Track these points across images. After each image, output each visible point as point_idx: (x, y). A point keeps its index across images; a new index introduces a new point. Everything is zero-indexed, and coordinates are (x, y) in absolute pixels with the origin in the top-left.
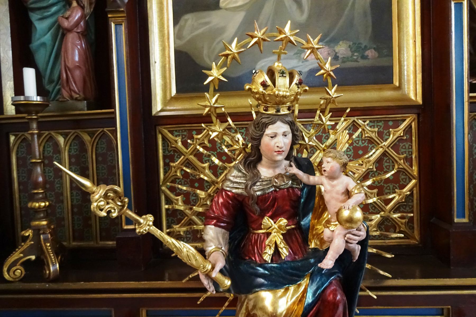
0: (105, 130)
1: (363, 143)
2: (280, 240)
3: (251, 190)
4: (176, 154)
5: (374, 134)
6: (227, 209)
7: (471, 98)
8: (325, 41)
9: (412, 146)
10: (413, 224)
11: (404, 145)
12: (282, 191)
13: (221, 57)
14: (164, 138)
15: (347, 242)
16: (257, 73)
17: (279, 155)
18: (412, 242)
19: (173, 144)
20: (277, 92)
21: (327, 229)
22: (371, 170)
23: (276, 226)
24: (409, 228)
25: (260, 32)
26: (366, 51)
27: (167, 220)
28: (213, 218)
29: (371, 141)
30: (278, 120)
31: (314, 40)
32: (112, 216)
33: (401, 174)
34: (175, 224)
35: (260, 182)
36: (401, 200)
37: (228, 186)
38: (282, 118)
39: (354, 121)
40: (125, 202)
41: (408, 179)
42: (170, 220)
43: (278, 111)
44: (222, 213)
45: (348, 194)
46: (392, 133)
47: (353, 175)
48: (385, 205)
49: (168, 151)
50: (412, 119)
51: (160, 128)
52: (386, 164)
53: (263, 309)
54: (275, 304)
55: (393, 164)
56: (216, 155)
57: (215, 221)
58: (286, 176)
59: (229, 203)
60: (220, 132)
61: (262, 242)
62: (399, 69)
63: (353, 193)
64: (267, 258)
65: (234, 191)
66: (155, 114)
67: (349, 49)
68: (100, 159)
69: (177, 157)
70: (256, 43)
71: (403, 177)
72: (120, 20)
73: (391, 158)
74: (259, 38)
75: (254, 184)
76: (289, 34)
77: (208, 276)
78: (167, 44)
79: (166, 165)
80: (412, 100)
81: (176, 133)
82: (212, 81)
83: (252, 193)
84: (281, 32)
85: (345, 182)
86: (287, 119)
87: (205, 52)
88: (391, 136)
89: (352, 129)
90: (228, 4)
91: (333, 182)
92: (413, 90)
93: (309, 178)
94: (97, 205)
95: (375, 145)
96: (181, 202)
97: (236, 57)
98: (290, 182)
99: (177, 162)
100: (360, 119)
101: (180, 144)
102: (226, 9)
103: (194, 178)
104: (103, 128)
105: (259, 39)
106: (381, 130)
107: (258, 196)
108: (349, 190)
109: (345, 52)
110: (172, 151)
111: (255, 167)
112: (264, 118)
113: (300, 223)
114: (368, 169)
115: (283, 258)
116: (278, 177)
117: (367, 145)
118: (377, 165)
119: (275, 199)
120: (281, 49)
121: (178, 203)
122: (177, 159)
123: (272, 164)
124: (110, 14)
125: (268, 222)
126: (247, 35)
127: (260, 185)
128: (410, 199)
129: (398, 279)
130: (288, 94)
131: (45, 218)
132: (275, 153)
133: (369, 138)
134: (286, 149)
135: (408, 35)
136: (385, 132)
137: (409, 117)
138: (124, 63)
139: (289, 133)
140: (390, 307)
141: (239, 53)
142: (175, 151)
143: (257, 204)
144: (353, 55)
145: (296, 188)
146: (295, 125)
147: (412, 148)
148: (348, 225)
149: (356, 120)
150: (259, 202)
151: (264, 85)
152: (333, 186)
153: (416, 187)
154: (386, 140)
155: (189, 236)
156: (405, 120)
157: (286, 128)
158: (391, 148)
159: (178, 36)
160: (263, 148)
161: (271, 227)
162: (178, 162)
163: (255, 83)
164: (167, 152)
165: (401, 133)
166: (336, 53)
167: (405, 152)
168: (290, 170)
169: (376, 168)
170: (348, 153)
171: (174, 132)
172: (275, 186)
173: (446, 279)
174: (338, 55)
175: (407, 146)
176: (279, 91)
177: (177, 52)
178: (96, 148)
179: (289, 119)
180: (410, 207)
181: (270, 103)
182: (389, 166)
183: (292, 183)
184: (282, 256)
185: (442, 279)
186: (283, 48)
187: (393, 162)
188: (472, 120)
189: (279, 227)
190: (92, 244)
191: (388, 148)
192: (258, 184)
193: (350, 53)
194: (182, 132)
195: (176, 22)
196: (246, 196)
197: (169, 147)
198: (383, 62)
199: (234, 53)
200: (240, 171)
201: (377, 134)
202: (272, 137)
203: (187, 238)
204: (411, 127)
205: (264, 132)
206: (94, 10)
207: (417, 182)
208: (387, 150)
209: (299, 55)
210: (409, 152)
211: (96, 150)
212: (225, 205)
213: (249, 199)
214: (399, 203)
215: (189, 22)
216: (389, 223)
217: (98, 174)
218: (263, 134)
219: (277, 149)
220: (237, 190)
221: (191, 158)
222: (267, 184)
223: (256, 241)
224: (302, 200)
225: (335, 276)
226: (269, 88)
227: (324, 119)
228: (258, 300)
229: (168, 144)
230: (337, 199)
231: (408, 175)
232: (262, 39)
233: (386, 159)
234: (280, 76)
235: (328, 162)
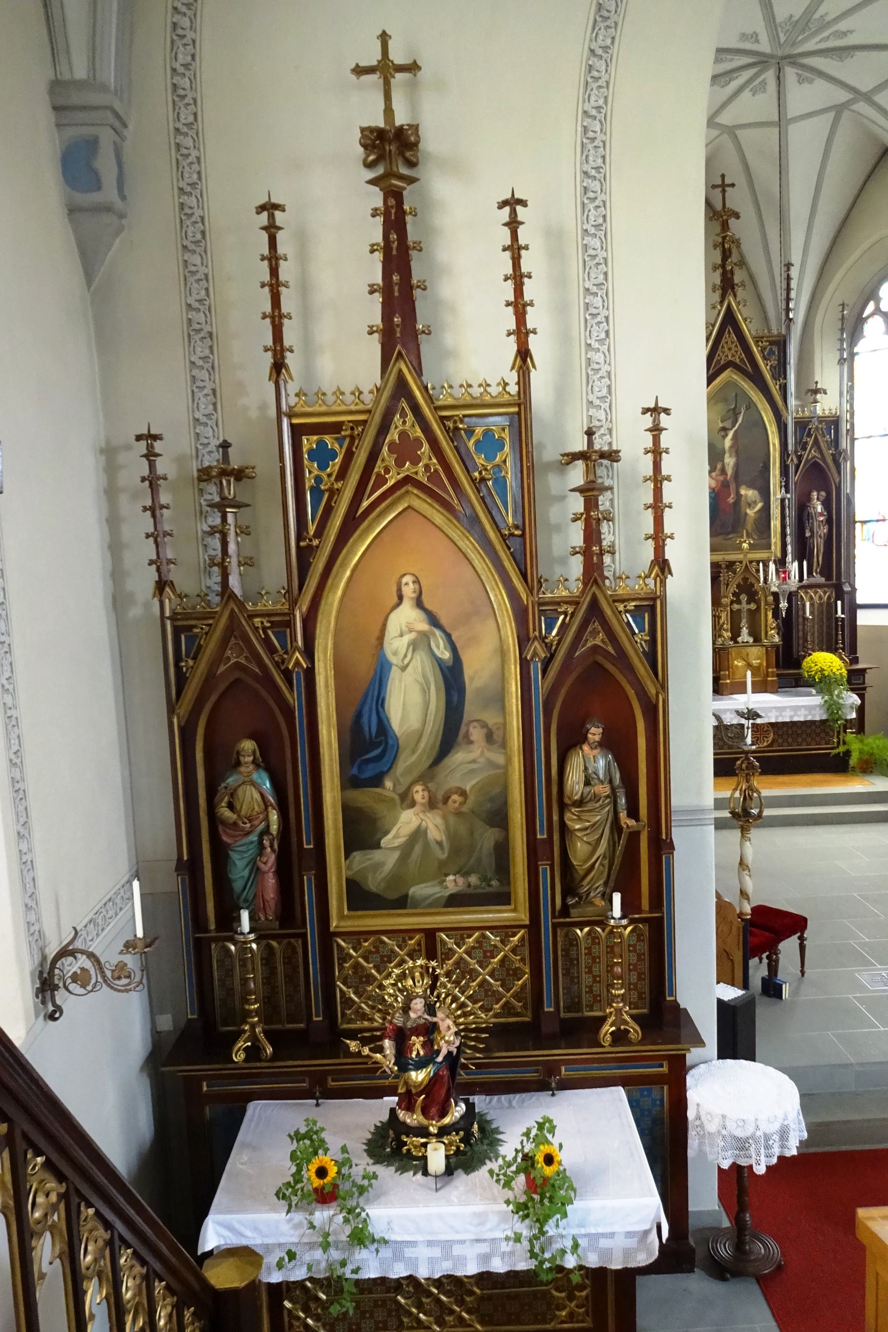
18: (527, 1019)
37: (395, 1021)
53: (412, 1079)
64: (414, 1056)
79: (340, 965)
87: (370, 878)
131: (256, 1016)
159: (349, 868)
177: (347, 879)
190: (279, 1027)
193: (479, 883)
195: (346, 859)
198: (504, 889)
212: (393, 1029)
228: (409, 1077)
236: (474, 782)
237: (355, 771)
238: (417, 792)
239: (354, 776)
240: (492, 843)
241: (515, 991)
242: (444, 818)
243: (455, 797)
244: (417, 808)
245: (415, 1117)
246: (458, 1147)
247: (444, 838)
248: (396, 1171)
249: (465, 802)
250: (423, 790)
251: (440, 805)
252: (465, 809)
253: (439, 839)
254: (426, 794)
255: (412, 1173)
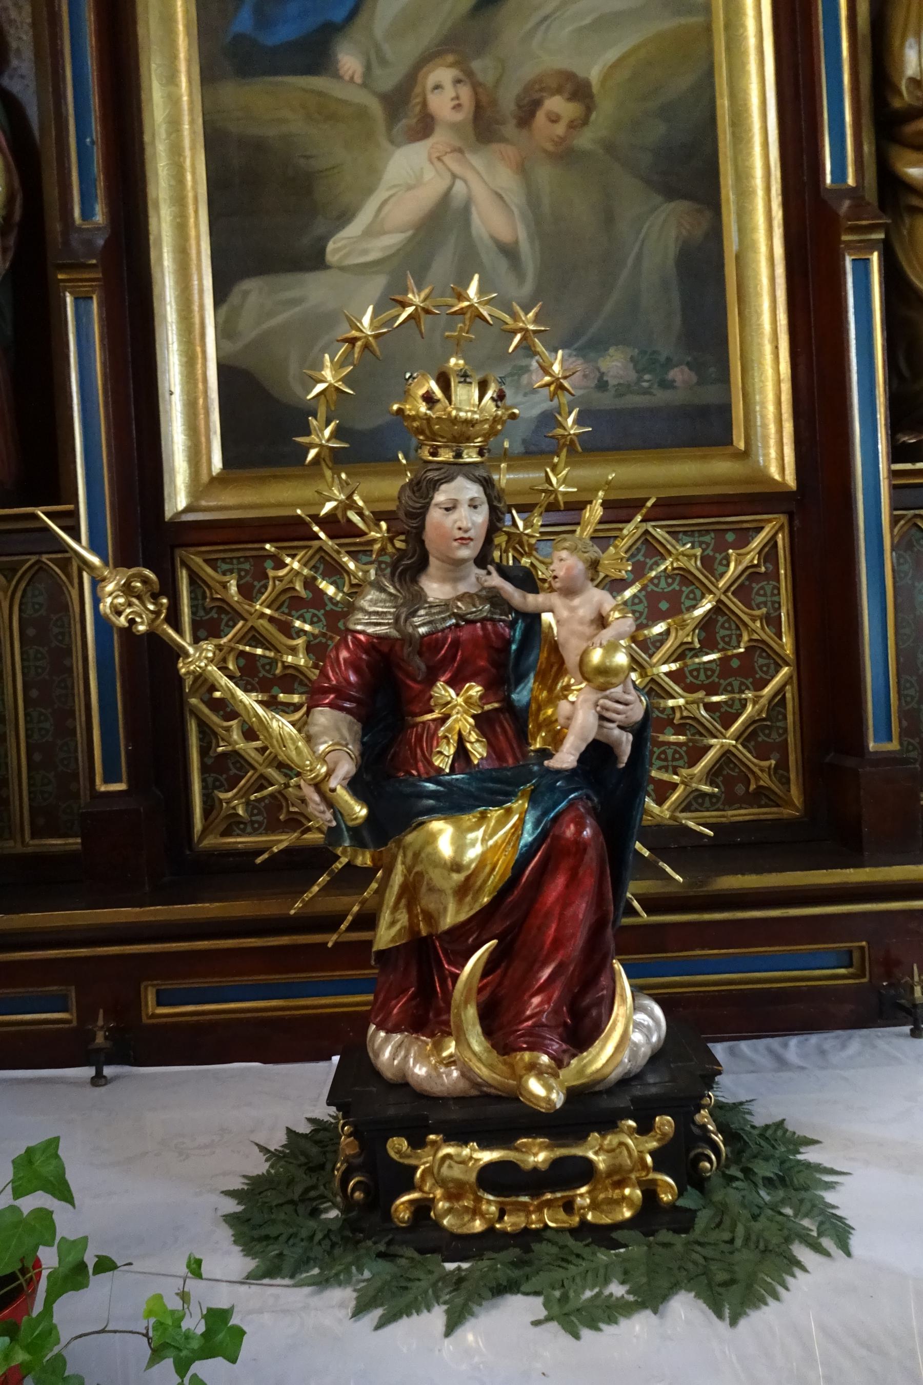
0: (44, 558)
1: (669, 585)
2: (468, 727)
3: (408, 624)
4: (223, 616)
5: (693, 562)
6: (357, 671)
7: (894, 474)
8: (576, 346)
9: (779, 589)
10: (788, 770)
11: (762, 588)
12: (470, 627)
13: (341, 344)
14: (195, 580)
15: (602, 718)
16: (414, 378)
17: (463, 547)
18: (787, 812)
19: (217, 593)
20: (454, 413)
21: (736, 1254)
22: (688, 646)
23: (460, 700)
24: (780, 781)
25: (419, 295)
26: (672, 368)
27: (203, 780)
28: (326, 691)
29: (685, 576)
30: (458, 475)
31: (526, 314)
32: (138, 631)
33: (758, 653)
34: (222, 789)
35: (425, 608)
36: (759, 715)
38: (468, 471)
39: (647, 532)
40: (162, 604)
41: (772, 666)
42: (210, 780)
43: (459, 455)
44: (347, 680)
45: (601, 622)
46: (733, 558)
47: (648, 659)
48: (723, 727)
49: (204, 609)
50: (776, 527)
51: (180, 553)
52: (723, 632)
54: (460, 846)
55: (738, 632)
56: (327, 601)
57: (332, 696)
58: (479, 597)
59: (361, 658)
60: (340, 502)
61: (433, 736)
62: (744, 409)
63: (611, 619)
65: (370, 630)
66: (171, 519)
67: (631, 365)
68: (31, 632)
69: (227, 625)
70: (410, 317)
71: (761, 661)
72: (85, 288)
73: (734, 618)
74: (417, 306)
75: (413, 614)
76: (475, 300)
77: (318, 786)
78: (199, 349)
80: (774, 480)
81: (225, 567)
82: (322, 393)
83: (410, 630)
84: (461, 297)
85: (596, 599)
86: (477, 474)
88: (732, 565)
89: (643, 552)
90: (347, 255)
91: (572, 600)
92: (776, 459)
93: (525, 598)
94: (112, 603)
95: (697, 588)
96: (238, 735)
97: (372, 346)
98: (487, 607)
99: (226, 635)
100: (661, 527)
101: (233, 589)
102: (343, 269)
103: (270, 676)
104: (40, 553)
105: (416, 309)
106: (709, 552)
107: (423, 636)
108: (604, 614)
109: (621, 372)
110: (214, 611)
111: (415, 580)
112: (430, 470)
113: (509, 696)
114: (682, 644)
115: (476, 762)
116: (460, 598)
117: (677, 588)
118: (703, 634)
119: (456, 644)
120: (461, 330)
121: (231, 736)
122: (226, 629)
123: (450, 571)
124: (61, 273)
125: (443, 692)
126: (394, 300)
127: (427, 614)
128: (779, 712)
129: (743, 874)
130: (477, 416)
132: (456, 544)
133: (681, 572)
134: (478, 533)
135: (761, 334)
136: (719, 557)
137: (770, 521)
138: (97, 390)
139: (483, 503)
140: (731, 951)
141: (376, 337)
142: (221, 610)
143: (420, 654)
144: (640, 379)
145: (501, 620)
146: (493, 486)
147: (779, 594)
148: (601, 680)
149: (651, 530)
150: (424, 649)
151: (429, 399)
152: (573, 609)
153: (791, 684)
154: (722, 575)
155: (259, 818)
156: (762, 528)
157: (474, 491)
158: (733, 593)
160: (430, 535)
161: (449, 703)
162: (230, 636)
163: (411, 399)
164: (201, 613)
165: (753, 559)
166: (602, 374)
167: (765, 604)
168: (486, 581)
169: (700, 641)
170: (636, 608)
171: (219, 563)
172: (455, 615)
173: (848, 871)
174: (605, 378)
175: (768, 589)
176: (459, 410)
177: (222, 369)
178: (21, 604)
179: (481, 472)
180: (781, 731)
181: (443, 437)
182: (730, 636)
183: (490, 611)
184: (472, 758)
185: (839, 870)
186: (467, 328)
187: (738, 628)
188: (910, 529)
189: (466, 702)
191: (725, 592)
192: (422, 612)
193: (633, 376)
194: (239, 563)
195: (220, 298)
196: (397, 639)
197: (208, 600)
198: (709, 395)
199: (367, 336)
200: (382, 589)
201: (699, 563)
202: (447, 509)
203: (252, 822)
204: (776, 543)
205: (432, 498)
206: (11, 266)
207: (791, 672)
208: (723, 598)
209: (516, 377)
210: (773, 602)
211: (20, 610)
212: (353, 664)
213: (402, 646)
214: (754, 722)
215: (253, 299)
216: (733, 770)
217: (26, 671)
218: (429, 503)
219: (460, 534)
220: (378, 628)
221: (262, 625)
222: (439, 613)
223: (419, 738)
224: (514, 647)
225: (580, 792)
226: (438, 406)
227: (554, 480)
229: (204, 592)
230: (581, 636)
231: (775, 657)
232: (423, 309)
233: (721, 619)
234: (460, 382)
235: (561, 560)
236: (612, 55)
237: (244, 22)
238: (437, 87)
239: (239, 39)
240: (672, 251)
241: (751, 722)
242: (523, 170)
243: (555, 104)
244: (440, 139)
245: (451, 1048)
246: (650, 1193)
247: (522, 235)
248: (359, 1311)
249: (585, 121)
250: (457, 81)
251: (510, 129)
252: (585, 140)
253: (505, 234)
254: (465, 93)
255: (437, 1317)
